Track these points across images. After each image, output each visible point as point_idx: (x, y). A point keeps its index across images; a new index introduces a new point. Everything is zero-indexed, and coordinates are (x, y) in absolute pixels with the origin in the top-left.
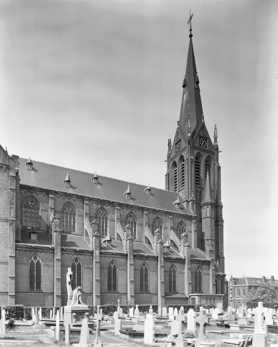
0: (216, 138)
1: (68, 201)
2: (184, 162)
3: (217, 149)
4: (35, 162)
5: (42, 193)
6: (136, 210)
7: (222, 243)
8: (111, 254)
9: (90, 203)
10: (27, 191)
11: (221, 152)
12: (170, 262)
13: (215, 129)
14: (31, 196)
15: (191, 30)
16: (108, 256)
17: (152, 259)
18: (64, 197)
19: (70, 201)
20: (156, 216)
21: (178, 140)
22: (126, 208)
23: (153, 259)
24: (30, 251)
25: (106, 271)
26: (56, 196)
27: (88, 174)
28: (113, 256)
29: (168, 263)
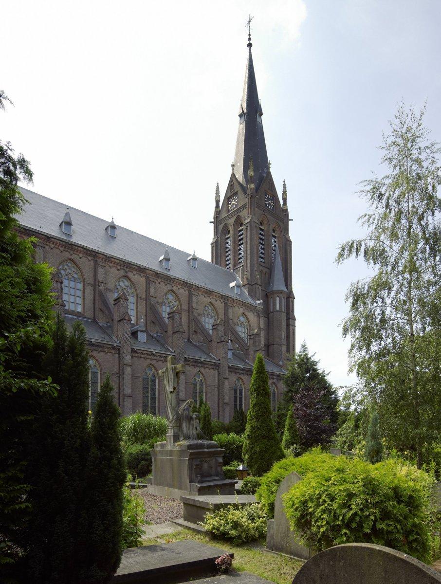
0: (285, 200)
1: (70, 257)
2: (241, 226)
3: (287, 215)
4: (119, 227)
5: (210, 297)
6: (179, 287)
7: (288, 350)
8: (109, 346)
9: (107, 266)
10: (64, 250)
11: (292, 220)
12: (236, 373)
13: (284, 185)
14: (172, 291)
15: (250, 39)
16: (144, 356)
17: (210, 367)
18: (62, 249)
19: (72, 258)
20: (169, 287)
21: (234, 192)
22: (165, 282)
23: (213, 367)
24: (144, 358)
25: (140, 384)
26: (47, 245)
27: (77, 210)
28: (153, 357)
29: (233, 374)
